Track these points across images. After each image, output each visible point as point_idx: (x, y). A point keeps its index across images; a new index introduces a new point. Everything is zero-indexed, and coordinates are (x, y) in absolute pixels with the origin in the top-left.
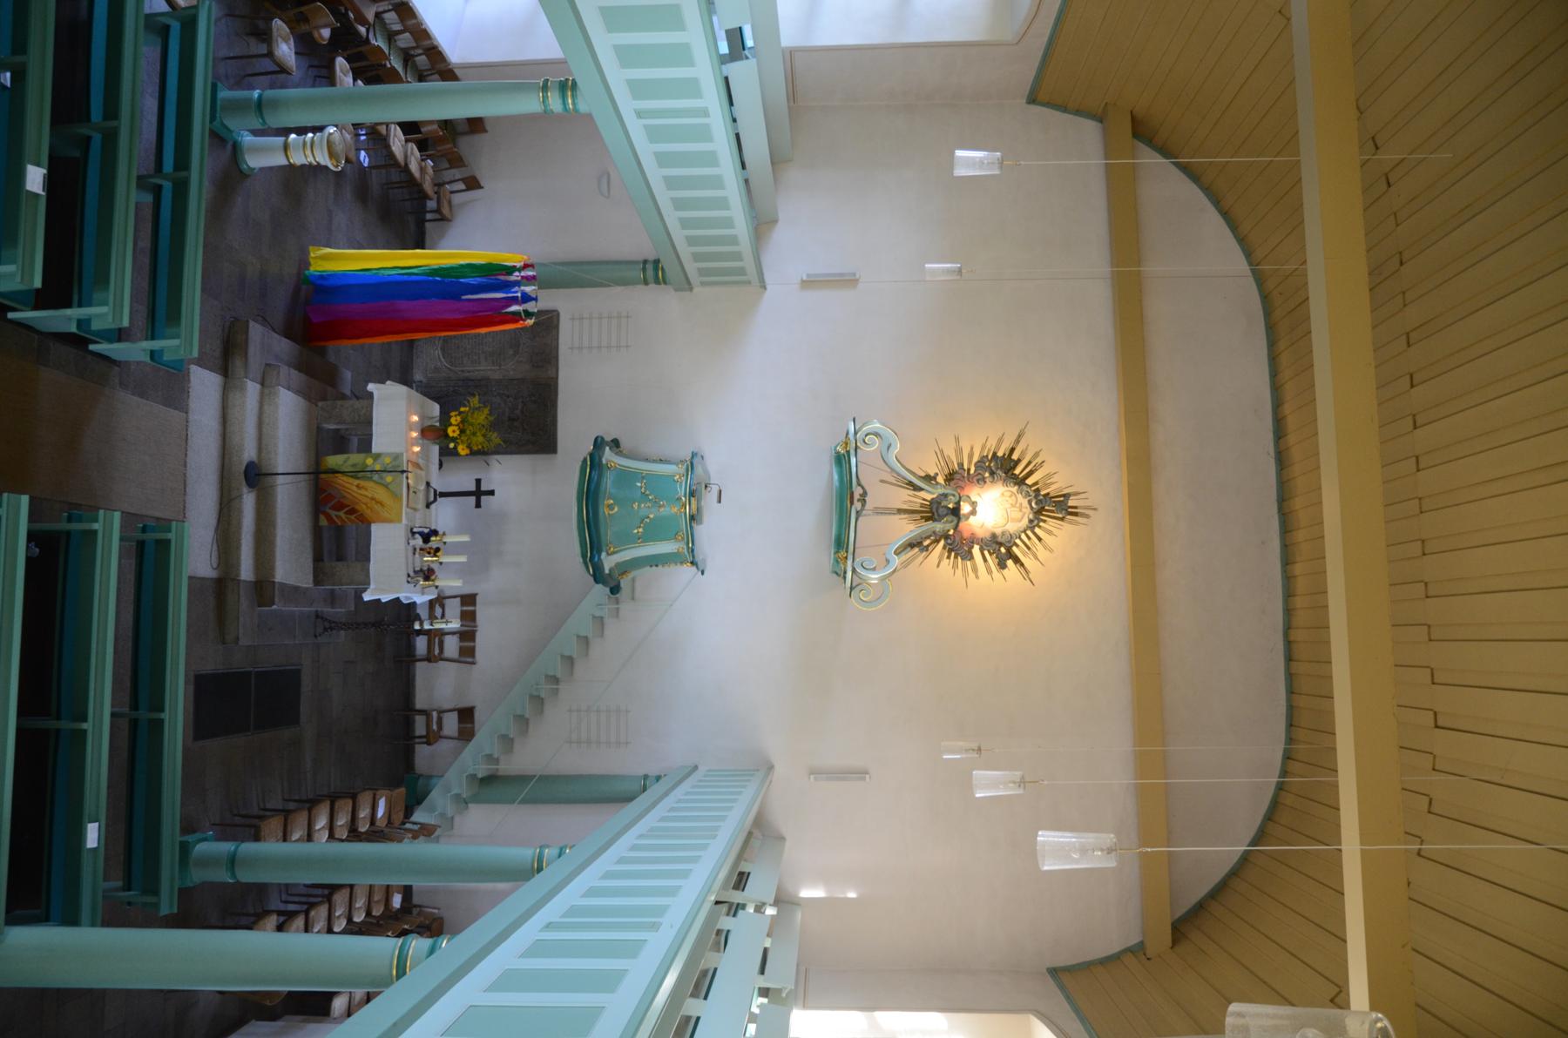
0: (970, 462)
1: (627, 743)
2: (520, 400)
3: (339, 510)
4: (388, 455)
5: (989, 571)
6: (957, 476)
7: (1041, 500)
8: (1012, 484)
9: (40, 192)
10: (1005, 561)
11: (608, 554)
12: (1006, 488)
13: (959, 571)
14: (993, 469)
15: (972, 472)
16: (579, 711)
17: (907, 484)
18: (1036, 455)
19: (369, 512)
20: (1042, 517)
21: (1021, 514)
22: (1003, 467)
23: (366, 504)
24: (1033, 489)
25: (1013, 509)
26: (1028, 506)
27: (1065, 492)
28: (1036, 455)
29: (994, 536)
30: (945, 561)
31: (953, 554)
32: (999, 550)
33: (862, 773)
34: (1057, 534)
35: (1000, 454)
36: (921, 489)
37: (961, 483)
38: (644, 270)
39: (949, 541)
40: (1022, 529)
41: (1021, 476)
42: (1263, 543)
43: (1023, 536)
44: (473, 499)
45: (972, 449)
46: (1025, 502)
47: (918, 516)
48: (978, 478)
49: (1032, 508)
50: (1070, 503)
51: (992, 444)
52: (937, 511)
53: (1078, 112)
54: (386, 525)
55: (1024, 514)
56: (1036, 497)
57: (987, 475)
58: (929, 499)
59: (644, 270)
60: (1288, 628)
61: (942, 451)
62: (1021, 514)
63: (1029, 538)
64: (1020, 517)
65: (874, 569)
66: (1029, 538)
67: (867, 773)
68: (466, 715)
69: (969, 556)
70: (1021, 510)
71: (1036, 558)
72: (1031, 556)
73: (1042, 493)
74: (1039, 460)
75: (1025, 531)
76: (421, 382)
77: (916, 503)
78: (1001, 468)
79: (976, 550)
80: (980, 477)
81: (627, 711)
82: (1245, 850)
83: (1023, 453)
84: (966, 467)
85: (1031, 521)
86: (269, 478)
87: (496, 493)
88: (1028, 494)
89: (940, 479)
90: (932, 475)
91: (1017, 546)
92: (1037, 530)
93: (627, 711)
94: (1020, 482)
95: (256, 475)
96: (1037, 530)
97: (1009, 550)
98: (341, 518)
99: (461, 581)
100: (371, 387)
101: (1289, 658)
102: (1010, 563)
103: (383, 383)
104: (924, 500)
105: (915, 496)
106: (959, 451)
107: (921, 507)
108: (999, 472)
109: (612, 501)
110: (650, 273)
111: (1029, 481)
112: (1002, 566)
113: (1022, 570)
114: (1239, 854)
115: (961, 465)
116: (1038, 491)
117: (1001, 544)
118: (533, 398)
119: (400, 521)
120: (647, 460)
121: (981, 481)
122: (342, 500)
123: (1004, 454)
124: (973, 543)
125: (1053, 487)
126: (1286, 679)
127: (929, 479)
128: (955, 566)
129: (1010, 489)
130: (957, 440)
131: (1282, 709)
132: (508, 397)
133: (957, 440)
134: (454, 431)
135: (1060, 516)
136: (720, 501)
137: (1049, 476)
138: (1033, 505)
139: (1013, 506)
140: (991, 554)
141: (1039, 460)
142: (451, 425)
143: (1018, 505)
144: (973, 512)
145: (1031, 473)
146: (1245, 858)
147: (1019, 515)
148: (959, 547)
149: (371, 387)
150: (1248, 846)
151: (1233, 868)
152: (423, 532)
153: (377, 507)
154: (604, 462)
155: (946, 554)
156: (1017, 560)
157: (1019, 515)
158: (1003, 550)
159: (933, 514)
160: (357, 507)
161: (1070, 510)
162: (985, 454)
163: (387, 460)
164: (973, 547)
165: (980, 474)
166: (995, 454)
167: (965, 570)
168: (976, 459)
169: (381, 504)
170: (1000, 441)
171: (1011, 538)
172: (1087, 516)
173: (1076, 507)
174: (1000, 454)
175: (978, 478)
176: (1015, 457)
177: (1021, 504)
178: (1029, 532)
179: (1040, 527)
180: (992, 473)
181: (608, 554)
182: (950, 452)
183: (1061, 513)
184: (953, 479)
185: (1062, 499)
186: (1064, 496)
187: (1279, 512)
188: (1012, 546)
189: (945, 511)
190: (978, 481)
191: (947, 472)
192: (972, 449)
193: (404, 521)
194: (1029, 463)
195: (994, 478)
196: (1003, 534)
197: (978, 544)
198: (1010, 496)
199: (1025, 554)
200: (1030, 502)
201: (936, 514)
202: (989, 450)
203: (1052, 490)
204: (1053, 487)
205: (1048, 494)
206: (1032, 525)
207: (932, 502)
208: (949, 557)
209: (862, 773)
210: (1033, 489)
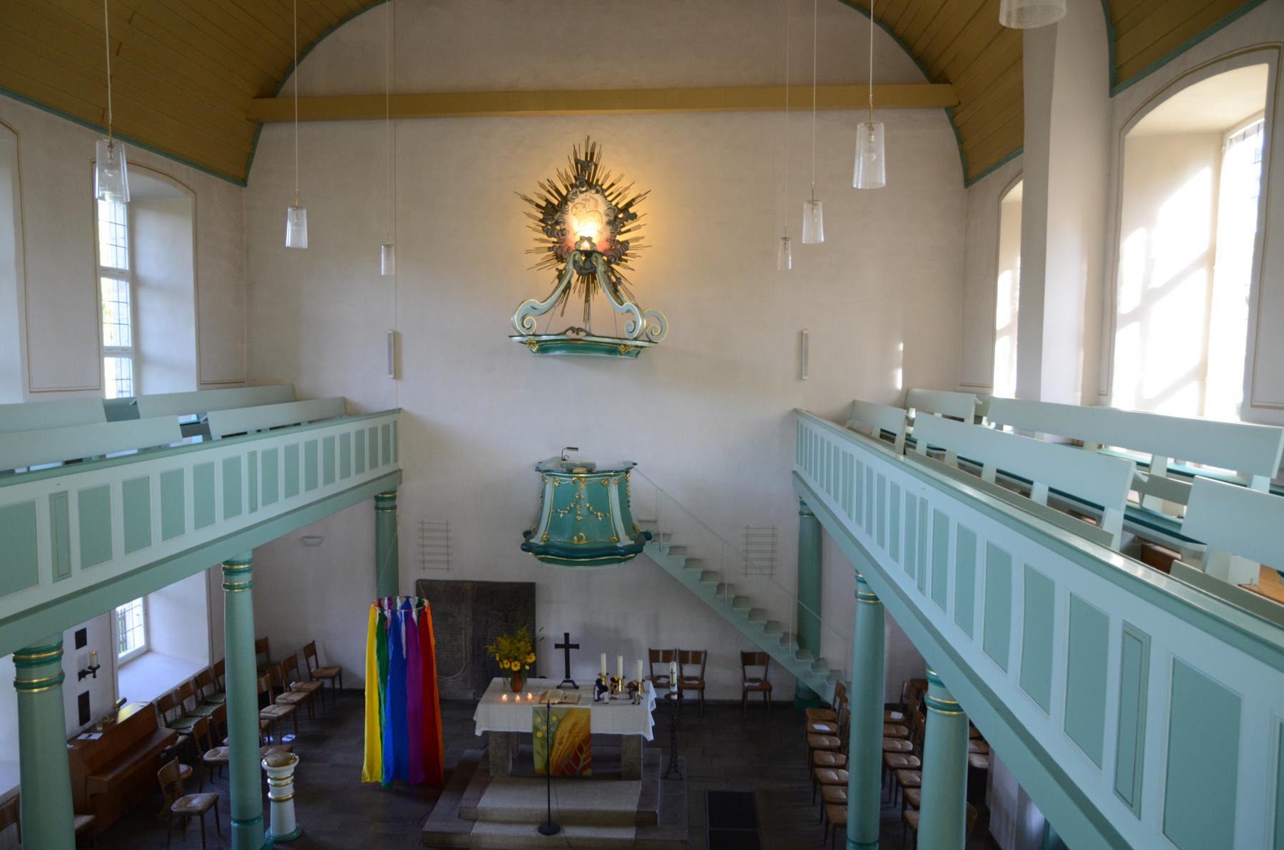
3: (579, 759)
4: (534, 718)
5: (639, 227)
6: (559, 252)
8: (567, 207)
15: (555, 240)
17: (565, 294)
18: (542, 186)
19: (580, 735)
21: (591, 200)
22: (552, 214)
23: (575, 738)
24: (570, 189)
25: (587, 205)
26: (585, 194)
27: (573, 162)
28: (542, 186)
29: (609, 223)
30: (629, 264)
32: (621, 219)
33: (802, 337)
34: (608, 170)
35: (541, 216)
36: (569, 283)
37: (565, 250)
38: (383, 509)
44: (571, 651)
45: (536, 239)
46: (582, 196)
47: (592, 286)
49: (586, 191)
50: (583, 158)
51: (533, 223)
53: (254, 144)
55: (593, 198)
56: (577, 187)
57: (558, 227)
59: (383, 509)
61: (538, 265)
63: (611, 194)
65: (635, 322)
66: (611, 194)
68: (748, 659)
69: (625, 244)
70: (588, 200)
71: (628, 188)
73: (574, 181)
74: (547, 184)
75: (606, 197)
76: (474, 693)
77: (580, 288)
78: (553, 216)
79: (620, 238)
80: (560, 234)
82: (874, 21)
83: (541, 197)
84: (551, 245)
85: (597, 192)
88: (575, 194)
89: (561, 266)
90: (557, 273)
91: (617, 204)
92: (605, 187)
94: (565, 200)
96: (605, 187)
97: (621, 211)
100: (478, 733)
102: (631, 210)
103: (474, 723)
105: (575, 287)
106: (538, 250)
107: (584, 282)
108: (556, 217)
110: (386, 504)
111: (564, 192)
112: (634, 217)
115: (550, 249)
116: (572, 186)
117: (616, 217)
119: (589, 709)
120: (542, 509)
123: (541, 212)
124: (614, 241)
127: (561, 276)
128: (634, 256)
130: (528, 252)
133: (528, 252)
134: (516, 666)
135: (593, 167)
136: (576, 449)
137: (560, 175)
138: (584, 189)
139: (584, 207)
140: (624, 226)
141: (547, 184)
143: (584, 202)
144: (589, 239)
145: (557, 191)
147: (592, 202)
148: (617, 252)
149: (478, 733)
150: (870, 18)
151: (887, 31)
153: (577, 729)
154: (542, 544)
155: (624, 263)
156: (630, 204)
157: (592, 202)
158: (621, 216)
160: (577, 745)
161: (588, 159)
162: (541, 228)
163: (539, 720)
164: (618, 241)
165: (557, 233)
166: (541, 221)
167: (636, 248)
168: (545, 237)
169: (574, 725)
170: (530, 215)
172: (594, 145)
173: (587, 154)
176: (543, 204)
177: (583, 200)
178: (607, 193)
179: (602, 185)
180: (557, 223)
181: (619, 541)
182: (539, 258)
184: (561, 256)
185: (579, 165)
188: (618, 208)
191: (555, 261)
192: (536, 239)
193: (589, 706)
194: (549, 192)
195: (562, 222)
196: (607, 215)
197: (616, 236)
198: (576, 208)
200: (581, 192)
203: (571, 174)
205: (575, 177)
206: (601, 191)
208: (626, 261)
209: (802, 337)
210: (570, 189)
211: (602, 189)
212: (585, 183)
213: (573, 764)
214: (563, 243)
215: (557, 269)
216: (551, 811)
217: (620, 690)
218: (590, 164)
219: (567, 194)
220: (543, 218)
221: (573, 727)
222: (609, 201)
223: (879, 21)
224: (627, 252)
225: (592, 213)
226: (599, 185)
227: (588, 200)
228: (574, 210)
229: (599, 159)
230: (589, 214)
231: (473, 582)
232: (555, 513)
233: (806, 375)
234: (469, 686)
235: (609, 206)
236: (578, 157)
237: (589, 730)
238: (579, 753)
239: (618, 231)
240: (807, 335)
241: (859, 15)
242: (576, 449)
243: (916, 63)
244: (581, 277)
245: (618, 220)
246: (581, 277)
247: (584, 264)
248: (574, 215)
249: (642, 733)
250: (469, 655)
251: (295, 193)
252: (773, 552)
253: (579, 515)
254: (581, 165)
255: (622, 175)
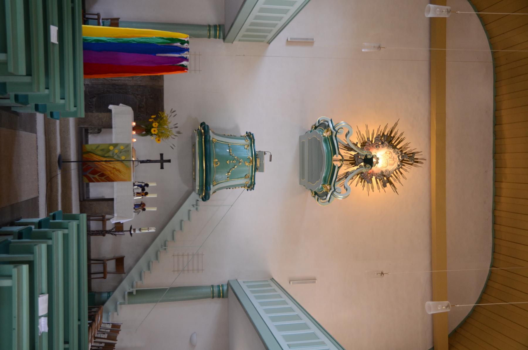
0: (372, 138)
1: (203, 270)
2: (145, 97)
3: (94, 174)
5: (379, 188)
6: (367, 144)
7: (403, 156)
8: (391, 148)
9: (57, 43)
10: (386, 183)
11: (213, 186)
12: (388, 150)
13: (365, 188)
14: (383, 141)
15: (373, 142)
16: (178, 255)
17: (344, 147)
18: (402, 134)
19: (112, 175)
20: (403, 164)
21: (394, 162)
23: (110, 171)
24: (400, 150)
25: (390, 159)
26: (398, 159)
27: (413, 152)
28: (402, 134)
29: (382, 172)
30: (360, 184)
31: (363, 180)
32: (384, 179)
33: (313, 280)
35: (386, 134)
37: (368, 147)
38: (209, 30)
39: (363, 175)
40: (395, 169)
41: (394, 144)
42: (486, 172)
43: (395, 173)
45: (374, 131)
46: (396, 156)
48: (376, 145)
51: (382, 128)
52: (357, 161)
54: (122, 183)
55: (395, 162)
56: (401, 154)
58: (353, 154)
59: (209, 30)
60: (494, 210)
61: (360, 132)
62: (394, 162)
64: (393, 163)
67: (316, 280)
68: (120, 261)
69: (370, 181)
70: (393, 160)
71: (400, 182)
72: (397, 181)
73: (404, 152)
74: (403, 137)
75: (395, 170)
76: (88, 85)
77: (348, 156)
79: (374, 179)
80: (377, 144)
81: (202, 255)
82: (474, 306)
84: (371, 140)
85: (399, 165)
86: (68, 163)
87: (171, 161)
88: (398, 153)
91: (392, 176)
92: (401, 170)
93: (202, 255)
94: (394, 147)
95: (63, 162)
96: (401, 170)
97: (388, 179)
98: (97, 179)
99: (156, 208)
100: (111, 107)
101: (494, 223)
102: (388, 184)
104: (351, 155)
105: (347, 153)
106: (368, 132)
107: (350, 158)
108: (386, 142)
109: (217, 160)
110: (212, 32)
111: (398, 147)
112: (384, 186)
113: (393, 188)
114: (472, 307)
115: (368, 139)
116: (401, 151)
117: (384, 176)
118: (151, 96)
119: (130, 180)
120: (224, 136)
121: (377, 146)
122: (96, 169)
123: (388, 134)
124: (373, 175)
125: (408, 150)
126: (492, 232)
128: (364, 186)
129: (390, 150)
130: (367, 126)
131: (491, 245)
132: (138, 95)
133: (367, 126)
134: (154, 131)
135: (411, 163)
136: (271, 161)
137: (407, 144)
140: (380, 180)
141: (403, 137)
142: (153, 127)
143: (392, 158)
144: (377, 163)
146: (474, 310)
149: (111, 107)
150: (475, 304)
151: (468, 314)
152: (141, 185)
154: (211, 139)
155: (360, 180)
156: (391, 183)
158: (385, 178)
159: (356, 162)
160: (104, 173)
161: (415, 160)
162: (379, 134)
163: (122, 147)
164: (372, 177)
165: (377, 143)
166: (383, 133)
168: (375, 136)
169: (119, 171)
171: (390, 173)
172: (422, 163)
173: (417, 159)
174: (386, 134)
175: (376, 145)
176: (392, 135)
177: (394, 157)
178: (397, 171)
179: (402, 168)
180: (382, 143)
181: (213, 186)
182: (364, 132)
183: (412, 162)
184: (365, 145)
185: (412, 155)
186: (412, 153)
187: (493, 158)
188: (390, 177)
189: (361, 160)
190: (376, 146)
191: (362, 142)
192: (374, 131)
193: (132, 181)
194: (398, 138)
195: (383, 145)
196: (386, 171)
197: (375, 176)
198: (389, 154)
199: (395, 180)
200: (398, 157)
201: (357, 162)
202: (381, 132)
204: (408, 150)
205: (406, 153)
207: (355, 155)
208: (361, 182)
209: (313, 280)
210: (400, 150)
211: (400, 168)
212: (403, 159)
213: (91, 170)
214: (372, 147)
215: (357, 143)
216: (70, 163)
217: (135, 198)
218: (412, 161)
219: (397, 148)
220: (385, 135)
221: (117, 170)
222: (393, 172)
223: (475, 307)
224: (366, 182)
225: (387, 163)
226: (402, 166)
227: (393, 160)
228: (388, 152)
229: (416, 166)
230: (386, 161)
231: (163, 86)
232: (228, 144)
233: (293, 283)
234: (93, 81)
235: (391, 172)
236: (416, 154)
237: (116, 181)
238: (99, 174)
239: (378, 178)
240: (315, 282)
241: (476, 299)
242: (271, 161)
243: (453, 331)
244: (353, 156)
245: (383, 177)
246: (353, 156)
247: (360, 158)
248: (386, 153)
249: (115, 215)
250: (113, 82)
251: (457, 11)
252: (188, 270)
253: (230, 162)
254: (412, 156)
255: (406, 179)
